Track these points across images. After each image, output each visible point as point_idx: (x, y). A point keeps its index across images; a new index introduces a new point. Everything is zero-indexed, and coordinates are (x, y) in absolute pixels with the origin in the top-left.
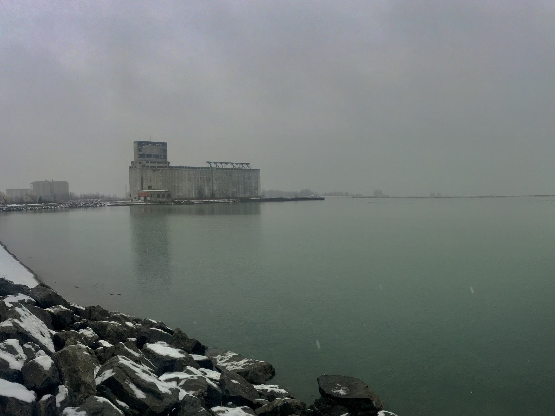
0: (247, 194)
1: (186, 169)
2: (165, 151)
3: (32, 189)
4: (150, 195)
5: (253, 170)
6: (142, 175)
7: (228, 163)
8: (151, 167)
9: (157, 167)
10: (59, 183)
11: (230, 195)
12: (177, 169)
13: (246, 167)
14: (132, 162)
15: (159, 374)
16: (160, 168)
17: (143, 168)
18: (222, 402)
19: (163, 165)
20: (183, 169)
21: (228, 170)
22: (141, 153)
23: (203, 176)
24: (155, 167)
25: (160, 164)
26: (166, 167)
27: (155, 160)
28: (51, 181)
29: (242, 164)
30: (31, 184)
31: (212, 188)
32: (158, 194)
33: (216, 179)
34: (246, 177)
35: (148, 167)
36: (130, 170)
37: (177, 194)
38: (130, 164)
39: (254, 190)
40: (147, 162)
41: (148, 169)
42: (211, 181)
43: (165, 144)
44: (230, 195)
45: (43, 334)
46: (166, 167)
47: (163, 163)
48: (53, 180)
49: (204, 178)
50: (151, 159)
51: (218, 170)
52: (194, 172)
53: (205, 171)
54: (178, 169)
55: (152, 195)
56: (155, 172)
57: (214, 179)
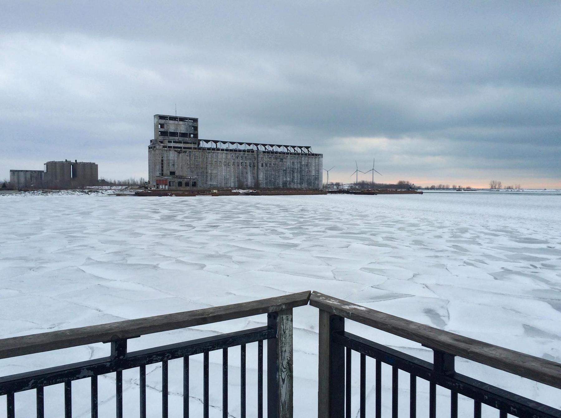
0: (303, 185)
1: (222, 152)
2: (196, 128)
3: (45, 171)
4: (168, 184)
5: (313, 155)
6: (162, 157)
7: (281, 146)
8: (174, 147)
9: (183, 148)
10: (84, 165)
11: (281, 186)
12: (210, 151)
13: (306, 151)
14: (151, 141)
16: (187, 150)
17: (164, 149)
18: (345, 348)
19: (192, 146)
20: (219, 152)
21: (278, 155)
22: (162, 130)
23: (245, 161)
24: (181, 148)
25: (188, 145)
26: (195, 148)
27: (181, 139)
28: (75, 162)
29: (286, 147)
30: (44, 164)
31: (257, 176)
32: (180, 182)
33: (262, 166)
34: (303, 163)
35: (170, 147)
36: (149, 151)
37: (209, 183)
39: (313, 180)
40: (170, 142)
41: (170, 150)
42: (256, 168)
43: (195, 120)
44: (281, 186)
46: (195, 148)
47: (191, 143)
48: (76, 161)
49: (246, 163)
50: (176, 138)
51: (265, 154)
52: (234, 156)
53: (248, 154)
54: (211, 152)
55: (171, 183)
56: (181, 155)
57: (260, 165)
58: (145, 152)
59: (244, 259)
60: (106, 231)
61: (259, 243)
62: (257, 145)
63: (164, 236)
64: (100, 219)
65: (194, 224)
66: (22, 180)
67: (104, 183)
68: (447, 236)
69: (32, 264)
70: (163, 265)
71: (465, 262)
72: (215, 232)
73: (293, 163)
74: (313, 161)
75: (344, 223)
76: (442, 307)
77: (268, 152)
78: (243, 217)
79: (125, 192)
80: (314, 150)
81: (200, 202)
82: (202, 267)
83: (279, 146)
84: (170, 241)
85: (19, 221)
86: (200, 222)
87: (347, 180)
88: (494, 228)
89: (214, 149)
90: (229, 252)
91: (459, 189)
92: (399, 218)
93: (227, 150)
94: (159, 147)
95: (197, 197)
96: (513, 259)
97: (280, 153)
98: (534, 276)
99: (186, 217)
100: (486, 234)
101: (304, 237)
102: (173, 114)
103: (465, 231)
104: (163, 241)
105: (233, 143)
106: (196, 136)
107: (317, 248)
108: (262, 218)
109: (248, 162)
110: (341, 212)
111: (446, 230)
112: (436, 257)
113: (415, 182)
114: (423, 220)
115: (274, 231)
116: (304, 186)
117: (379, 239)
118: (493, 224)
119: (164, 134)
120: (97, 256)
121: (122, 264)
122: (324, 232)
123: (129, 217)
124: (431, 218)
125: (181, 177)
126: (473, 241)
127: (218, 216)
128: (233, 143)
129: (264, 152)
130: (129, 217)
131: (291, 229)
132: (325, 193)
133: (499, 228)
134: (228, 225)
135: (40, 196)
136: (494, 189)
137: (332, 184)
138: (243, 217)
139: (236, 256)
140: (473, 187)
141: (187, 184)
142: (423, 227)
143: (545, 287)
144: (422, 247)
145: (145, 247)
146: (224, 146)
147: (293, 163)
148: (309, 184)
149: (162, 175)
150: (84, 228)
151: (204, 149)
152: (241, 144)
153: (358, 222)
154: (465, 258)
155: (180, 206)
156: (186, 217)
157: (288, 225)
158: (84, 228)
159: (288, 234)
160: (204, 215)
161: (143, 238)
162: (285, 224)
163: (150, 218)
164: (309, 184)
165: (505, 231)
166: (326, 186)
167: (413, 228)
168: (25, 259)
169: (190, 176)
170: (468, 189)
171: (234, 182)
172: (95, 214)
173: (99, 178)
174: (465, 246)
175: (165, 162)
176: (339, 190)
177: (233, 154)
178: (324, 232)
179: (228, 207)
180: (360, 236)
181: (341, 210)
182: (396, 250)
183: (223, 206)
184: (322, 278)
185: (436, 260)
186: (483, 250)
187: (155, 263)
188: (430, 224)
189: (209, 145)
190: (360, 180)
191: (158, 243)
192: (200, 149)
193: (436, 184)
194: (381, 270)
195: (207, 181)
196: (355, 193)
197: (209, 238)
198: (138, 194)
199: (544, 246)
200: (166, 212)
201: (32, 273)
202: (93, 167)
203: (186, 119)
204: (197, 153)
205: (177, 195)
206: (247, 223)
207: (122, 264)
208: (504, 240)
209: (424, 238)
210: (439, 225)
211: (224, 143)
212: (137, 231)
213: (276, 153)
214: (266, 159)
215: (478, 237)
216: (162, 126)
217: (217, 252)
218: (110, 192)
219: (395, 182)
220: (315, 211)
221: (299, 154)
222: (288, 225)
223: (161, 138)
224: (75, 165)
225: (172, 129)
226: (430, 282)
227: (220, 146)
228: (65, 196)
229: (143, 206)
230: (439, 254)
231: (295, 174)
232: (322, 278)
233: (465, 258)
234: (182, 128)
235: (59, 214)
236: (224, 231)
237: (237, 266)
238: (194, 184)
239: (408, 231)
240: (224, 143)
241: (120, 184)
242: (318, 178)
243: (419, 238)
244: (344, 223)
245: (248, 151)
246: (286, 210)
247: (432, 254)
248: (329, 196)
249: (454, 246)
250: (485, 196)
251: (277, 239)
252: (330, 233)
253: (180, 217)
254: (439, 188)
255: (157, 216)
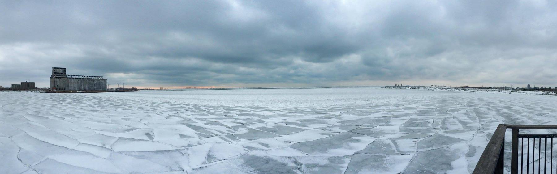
2: (65, 71)
8: (59, 77)
11: (93, 90)
13: (101, 78)
15: (432, 147)
19: (64, 77)
22: (55, 72)
27: (61, 75)
29: (95, 77)
33: (87, 83)
37: (69, 89)
38: (50, 76)
40: (57, 76)
43: (65, 69)
44: (93, 90)
45: (466, 89)
50: (59, 75)
57: (86, 83)
58: (49, 79)
59: (79, 116)
60: (34, 104)
61: (85, 110)
62: (85, 76)
63: (52, 107)
64: (33, 100)
65: (63, 103)
66: (15, 87)
67: (37, 88)
68: (150, 105)
69: (10, 113)
70: (50, 117)
71: (157, 114)
72: (70, 106)
73: (97, 82)
74: (104, 81)
75: (115, 102)
76: (151, 132)
77: (89, 79)
78: (80, 100)
79: (43, 92)
80: (104, 78)
81: (66, 95)
82: (64, 119)
83: (92, 77)
84: (54, 109)
85: (11, 99)
86: (65, 102)
87: (115, 87)
88: (163, 101)
89: (71, 78)
90: (74, 113)
91: (151, 90)
92: (133, 100)
93: (75, 78)
94: (54, 77)
95: (65, 94)
96: (171, 111)
97: (93, 79)
98: (179, 116)
99: (61, 100)
100: (161, 104)
101: (101, 107)
102: (58, 67)
103: (155, 103)
104: (52, 108)
105: (77, 76)
106: (65, 73)
107: (105, 112)
108: (86, 101)
109: (82, 82)
110: (113, 98)
111: (149, 103)
112: (147, 113)
113: (137, 88)
114: (141, 100)
115: (90, 106)
116: (101, 89)
117: (127, 107)
118: (163, 100)
119: (55, 73)
120: (30, 112)
121: (37, 116)
122: (108, 105)
123: (43, 100)
124: (144, 99)
125: (60, 87)
126: (158, 106)
127: (71, 100)
128: (77, 76)
129: (87, 79)
130: (43, 100)
131: (96, 105)
132: (108, 92)
133: (165, 101)
134: (75, 103)
135: (19, 92)
136: (161, 90)
137: (110, 89)
138: (80, 100)
139: (77, 115)
140: (155, 89)
141: (62, 89)
142: (141, 102)
143: (182, 119)
144: (141, 109)
145: (45, 110)
146: (74, 77)
147: (97, 82)
148: (103, 89)
149: (54, 86)
150: (28, 102)
151: (68, 78)
152: (80, 76)
153: (119, 101)
154: (156, 112)
155: (59, 97)
156: (61, 100)
157: (95, 103)
158: (28, 102)
159: (95, 106)
160: (67, 100)
161: (46, 107)
162: (94, 103)
163: (49, 100)
164: (103, 89)
165: (166, 102)
166: (108, 89)
167: (138, 103)
168: (9, 111)
169: (63, 87)
170: (154, 90)
171: (78, 89)
172: (32, 98)
173: (36, 87)
174: (155, 108)
175: (55, 82)
176: (112, 91)
177: (77, 79)
178: (108, 105)
179: (75, 97)
180: (120, 106)
181: (113, 97)
182: (133, 111)
183: (73, 97)
184: (108, 123)
185: (147, 114)
186: (162, 109)
187: (47, 116)
188: (143, 101)
189: (69, 77)
190: (119, 87)
191: (50, 109)
192: (67, 78)
193: (144, 89)
194: (129, 119)
195: (69, 88)
196: (118, 92)
197: (67, 108)
198: (46, 92)
199: (179, 106)
200: (54, 98)
201: (9, 116)
202: (34, 84)
203: (62, 68)
204: (66, 79)
205: (59, 93)
206: (81, 103)
207: (37, 116)
208: (167, 105)
209: (142, 106)
210: (146, 101)
211: (74, 76)
212: (44, 105)
213: (91, 79)
214: (88, 81)
215: (159, 105)
216: (55, 71)
217: (70, 113)
218: (38, 91)
219: (131, 88)
220: (105, 98)
221: (99, 79)
222: (95, 103)
223: (54, 74)
224: (29, 83)
225: (58, 71)
226: (146, 122)
227: (73, 77)
228: (26, 92)
229: (48, 96)
230: (148, 111)
231: (98, 86)
232: (108, 123)
233: (156, 112)
234: (61, 71)
235: (22, 98)
236: (73, 106)
237: (76, 119)
238: (64, 89)
239: (137, 104)
240: (74, 76)
241: (41, 89)
242: (106, 87)
243: (141, 106)
244: (115, 102)
245: (82, 78)
246: (95, 98)
247: (146, 112)
248: (109, 93)
249: (152, 108)
250: (159, 92)
251: (92, 108)
252: (110, 105)
253: (58, 100)
254: (145, 90)
255: (51, 100)
